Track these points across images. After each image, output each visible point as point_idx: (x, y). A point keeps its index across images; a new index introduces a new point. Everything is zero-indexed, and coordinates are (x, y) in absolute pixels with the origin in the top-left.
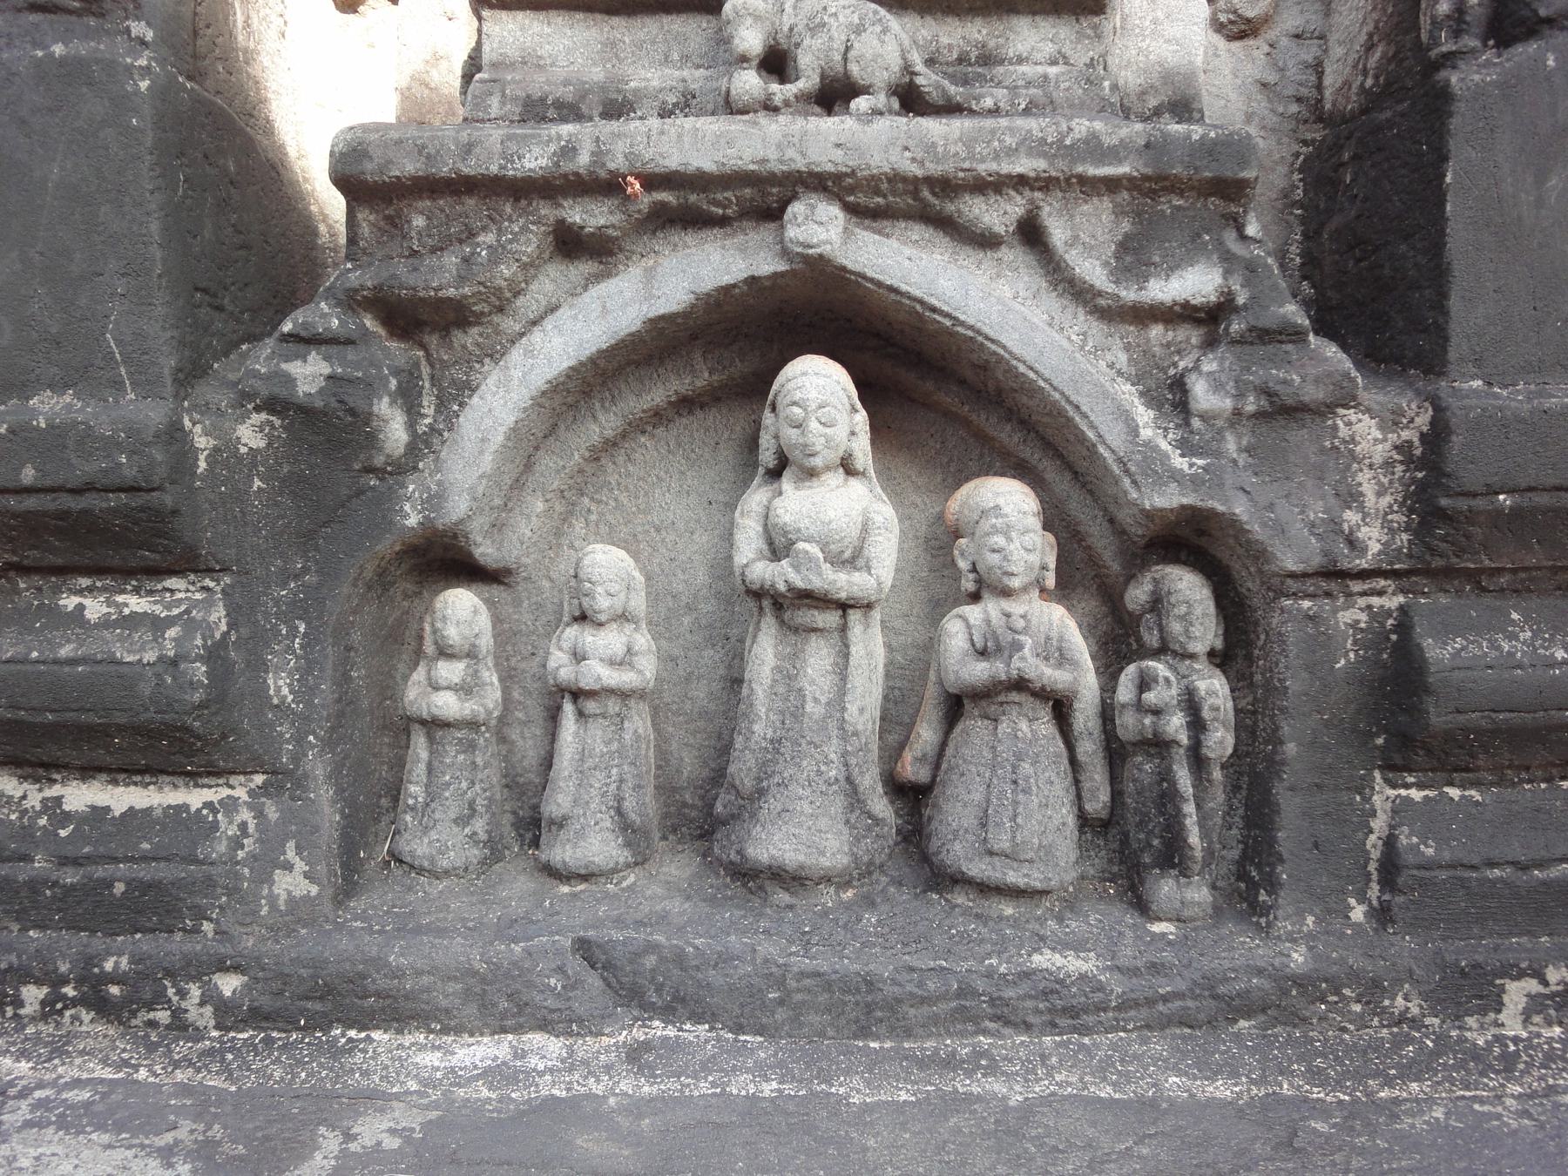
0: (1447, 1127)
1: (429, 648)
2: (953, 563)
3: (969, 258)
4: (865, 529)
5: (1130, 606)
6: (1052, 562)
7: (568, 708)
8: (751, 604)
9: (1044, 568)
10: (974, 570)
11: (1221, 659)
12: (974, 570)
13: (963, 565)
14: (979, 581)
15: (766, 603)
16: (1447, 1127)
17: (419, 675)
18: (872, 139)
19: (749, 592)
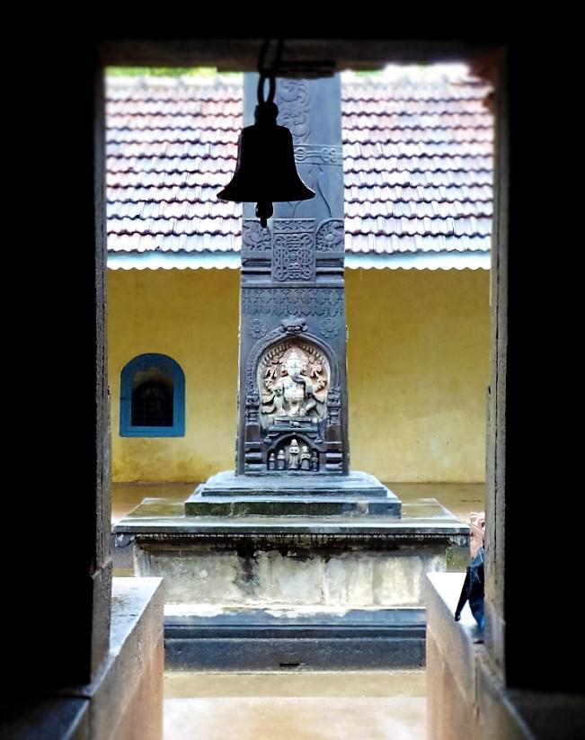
18: (297, 429)
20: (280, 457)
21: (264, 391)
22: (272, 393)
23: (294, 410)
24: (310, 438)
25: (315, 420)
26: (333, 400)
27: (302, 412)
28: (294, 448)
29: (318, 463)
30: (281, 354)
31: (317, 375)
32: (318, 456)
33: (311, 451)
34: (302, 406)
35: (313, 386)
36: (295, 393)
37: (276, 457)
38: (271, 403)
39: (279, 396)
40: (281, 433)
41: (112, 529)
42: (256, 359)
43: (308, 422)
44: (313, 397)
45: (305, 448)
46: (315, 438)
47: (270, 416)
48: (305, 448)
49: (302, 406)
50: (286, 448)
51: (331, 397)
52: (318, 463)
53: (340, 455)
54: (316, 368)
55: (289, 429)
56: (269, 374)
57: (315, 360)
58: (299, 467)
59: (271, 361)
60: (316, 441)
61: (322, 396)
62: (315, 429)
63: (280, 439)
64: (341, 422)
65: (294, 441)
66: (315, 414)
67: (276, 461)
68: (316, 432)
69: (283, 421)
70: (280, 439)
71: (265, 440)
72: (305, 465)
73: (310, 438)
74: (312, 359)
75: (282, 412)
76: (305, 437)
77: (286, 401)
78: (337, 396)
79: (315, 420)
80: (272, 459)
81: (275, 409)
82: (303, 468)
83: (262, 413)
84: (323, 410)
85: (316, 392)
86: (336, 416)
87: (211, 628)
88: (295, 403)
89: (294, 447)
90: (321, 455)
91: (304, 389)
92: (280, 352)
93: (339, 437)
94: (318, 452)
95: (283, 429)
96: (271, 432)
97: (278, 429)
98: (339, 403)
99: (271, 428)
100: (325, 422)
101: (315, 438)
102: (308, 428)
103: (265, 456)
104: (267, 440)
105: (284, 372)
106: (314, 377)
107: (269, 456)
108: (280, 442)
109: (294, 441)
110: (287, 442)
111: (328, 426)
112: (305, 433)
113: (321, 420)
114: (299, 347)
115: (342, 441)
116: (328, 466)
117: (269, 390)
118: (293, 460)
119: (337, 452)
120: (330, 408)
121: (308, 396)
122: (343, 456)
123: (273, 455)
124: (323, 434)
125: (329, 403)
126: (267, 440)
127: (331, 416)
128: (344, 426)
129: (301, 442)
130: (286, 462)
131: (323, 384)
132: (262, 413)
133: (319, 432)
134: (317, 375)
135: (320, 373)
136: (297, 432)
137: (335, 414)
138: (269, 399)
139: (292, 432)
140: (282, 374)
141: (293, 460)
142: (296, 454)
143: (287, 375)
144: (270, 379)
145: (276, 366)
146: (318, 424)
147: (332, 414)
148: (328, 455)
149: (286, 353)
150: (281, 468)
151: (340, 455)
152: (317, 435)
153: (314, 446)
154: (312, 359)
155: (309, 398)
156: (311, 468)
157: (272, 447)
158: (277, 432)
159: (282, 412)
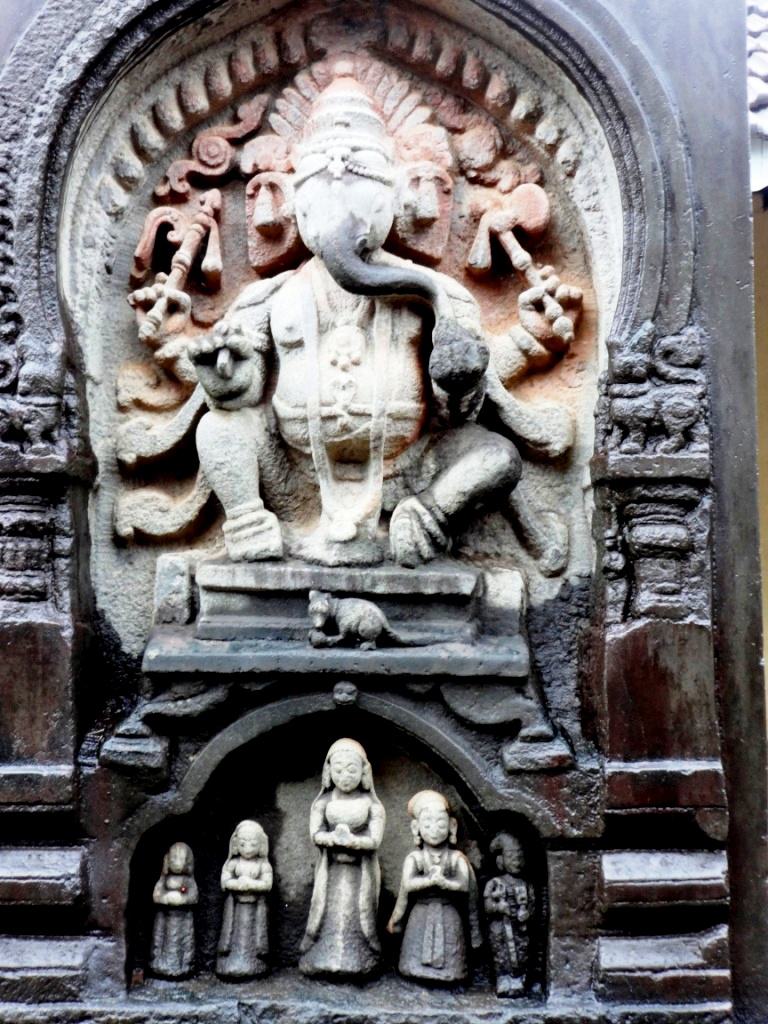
0: (139, 677)
1: (166, 871)
2: (410, 830)
3: (424, 648)
4: (369, 816)
5: (227, 880)
6: (454, 831)
7: (230, 899)
8: (317, 850)
9: (450, 834)
10: (419, 834)
11: (522, 875)
12: (419, 834)
13: (415, 832)
14: (422, 841)
15: (325, 851)
16: (139, 677)
17: (159, 885)
18: (365, 657)
19: (317, 845)
20: (245, 873)
21: (135, 383)
22: (185, 390)
23: (346, 506)
24: (463, 724)
25: (506, 588)
26: (653, 429)
27: (407, 531)
28: (346, 810)
29: (536, 932)
30: (250, 111)
31: (519, 256)
32: (533, 872)
33: (475, 824)
34: (407, 482)
35: (489, 335)
36: (350, 371)
37: (579, 615)
38: (175, 466)
39: (227, 399)
40: (242, 690)
41: (558, 720)
42: (44, 111)
43: (454, 602)
44: (493, 419)
45: (430, 809)
46: (508, 731)
47: (168, 559)
48: (430, 809)
49: (407, 482)
50: (286, 798)
51: (645, 400)
52: (536, 932)
53: (710, 870)
54: (514, 202)
55: (299, 656)
56: (163, 251)
57: (503, 153)
58: (384, 957)
59: (182, 165)
60: (514, 753)
61: (559, 411)
62: (510, 654)
63: (230, 738)
64: (718, 603)
65: (346, 757)
66: (510, 546)
67: (210, 908)
68: (517, 685)
69: (262, 598)
70: (230, 738)
71: (112, 745)
72: (432, 941)
73: (463, 724)
74: (477, 145)
75: (252, 527)
76: (431, 726)
77: (285, 450)
78: (680, 398)
79: (506, 588)
80: (172, 893)
81: (211, 514)
82: (412, 966)
83: (119, 543)
84: (565, 521)
85: (514, 383)
86: (680, 553)
87: (23, 882)
88: (350, 457)
89: (343, 798)
90: (556, 864)
91: (422, 346)
92: (244, 92)
93: (703, 722)
94: (536, 845)
95: (255, 656)
96: (165, 681)
97: (216, 654)
98: (699, 452)
99: (168, 650)
100: (584, 602)
101: (508, 731)
102: (452, 647)
103: (115, 863)
104: (130, 742)
105: (272, 233)
106: (495, 278)
107: (147, 867)
108: (233, 760)
109: (346, 757)
110: (294, 758)
111: (617, 633)
112: (433, 688)
113: (546, 591)
114: (398, 60)
115: (730, 752)
116: (618, 954)
117: (167, 373)
118: (340, 904)
119: (684, 838)
120: (621, 494)
121: (453, 405)
122: (733, 872)
123: (179, 855)
124: (564, 695)
125: (621, 456)
126: (130, 742)
127: (635, 555)
128: (738, 642)
129: (398, 760)
130: (285, 913)
131: (564, 323)
132: (119, 543)
133: (535, 679)
134: (519, 256)
135: (541, 242)
136: (368, 682)
137: (671, 534)
138: (157, 435)
139: (323, 680)
140: (260, 255)
141: (340, 904)
142: (359, 857)
143: (299, 255)
144: (169, 286)
145: (213, 196)
146: (531, 622)
147: (645, 533)
148: (624, 868)
149: (289, 103)
150: (239, 964)
151: (710, 870)
152: (522, 705)
153: (496, 786)
154: (477, 145)
155: (458, 421)
156: (477, 971)
157: (176, 799)
158: (202, 680)
159: (252, 527)
